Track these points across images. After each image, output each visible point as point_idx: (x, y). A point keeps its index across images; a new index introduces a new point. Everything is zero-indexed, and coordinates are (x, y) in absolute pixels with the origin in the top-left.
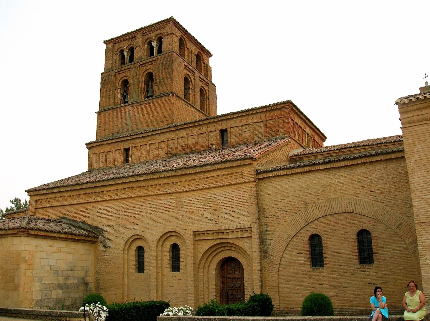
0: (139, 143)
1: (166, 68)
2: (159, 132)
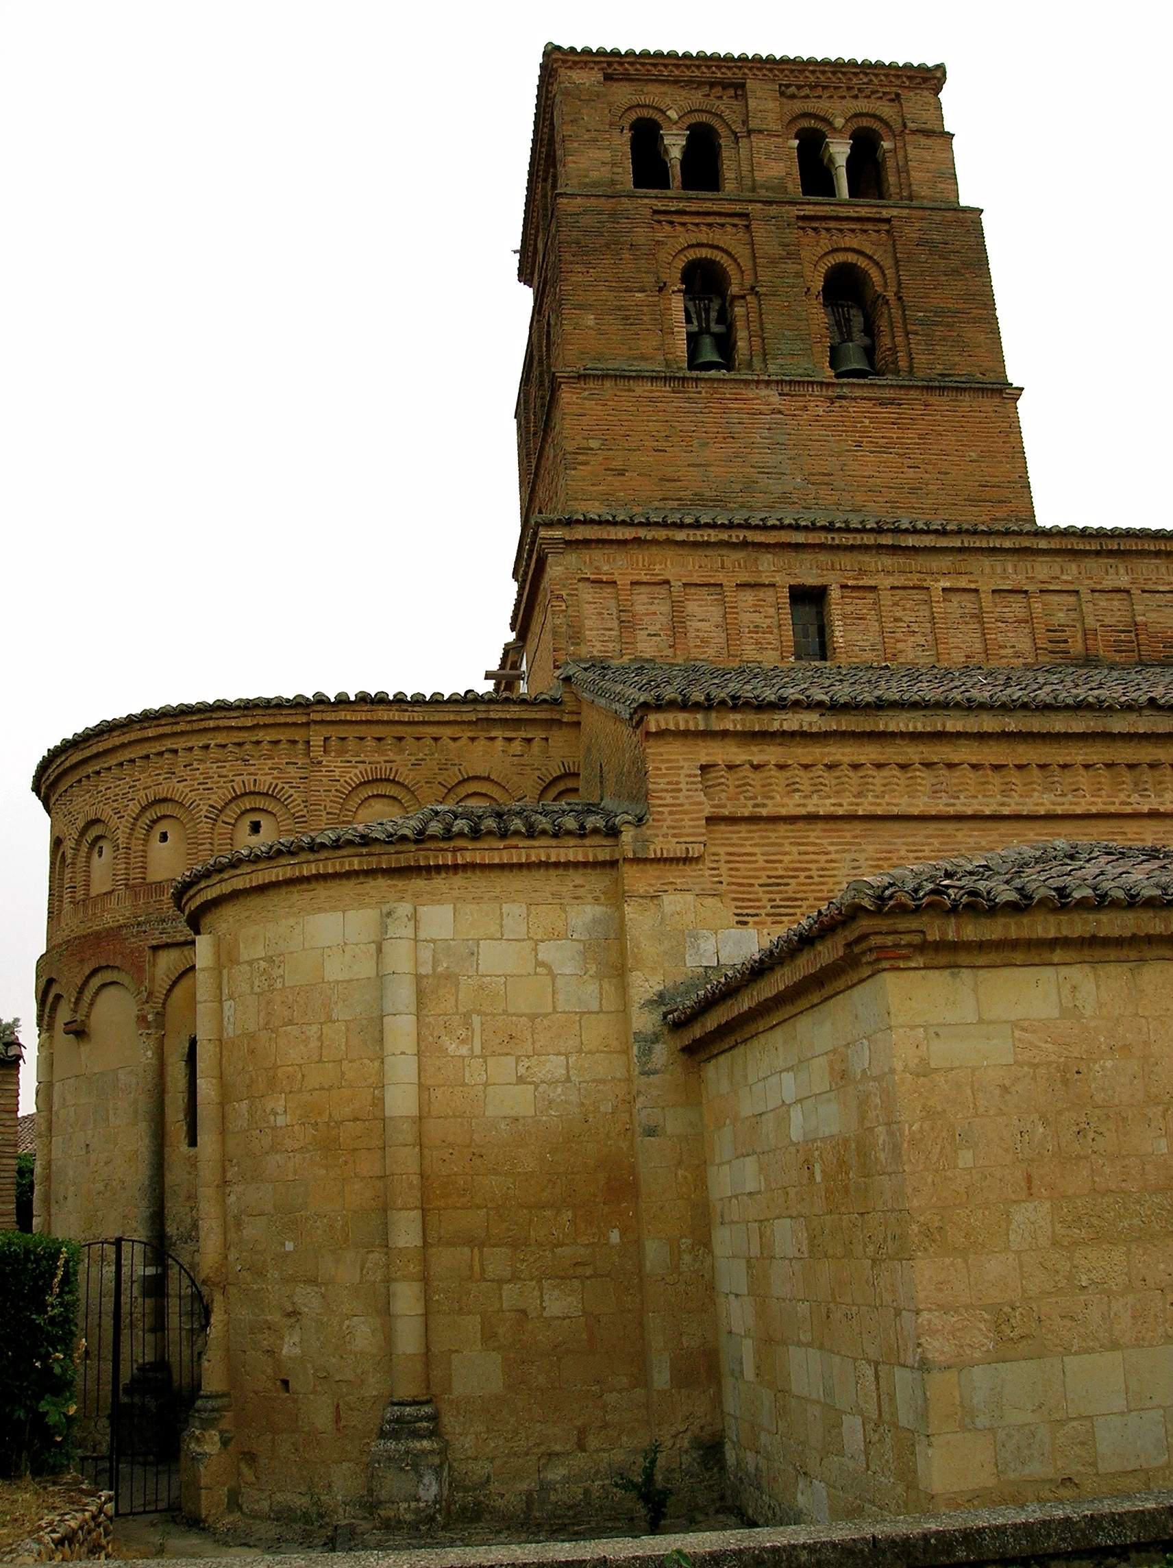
0: (883, 572)
1: (955, 272)
2: (1007, 543)
